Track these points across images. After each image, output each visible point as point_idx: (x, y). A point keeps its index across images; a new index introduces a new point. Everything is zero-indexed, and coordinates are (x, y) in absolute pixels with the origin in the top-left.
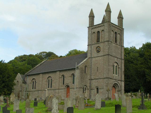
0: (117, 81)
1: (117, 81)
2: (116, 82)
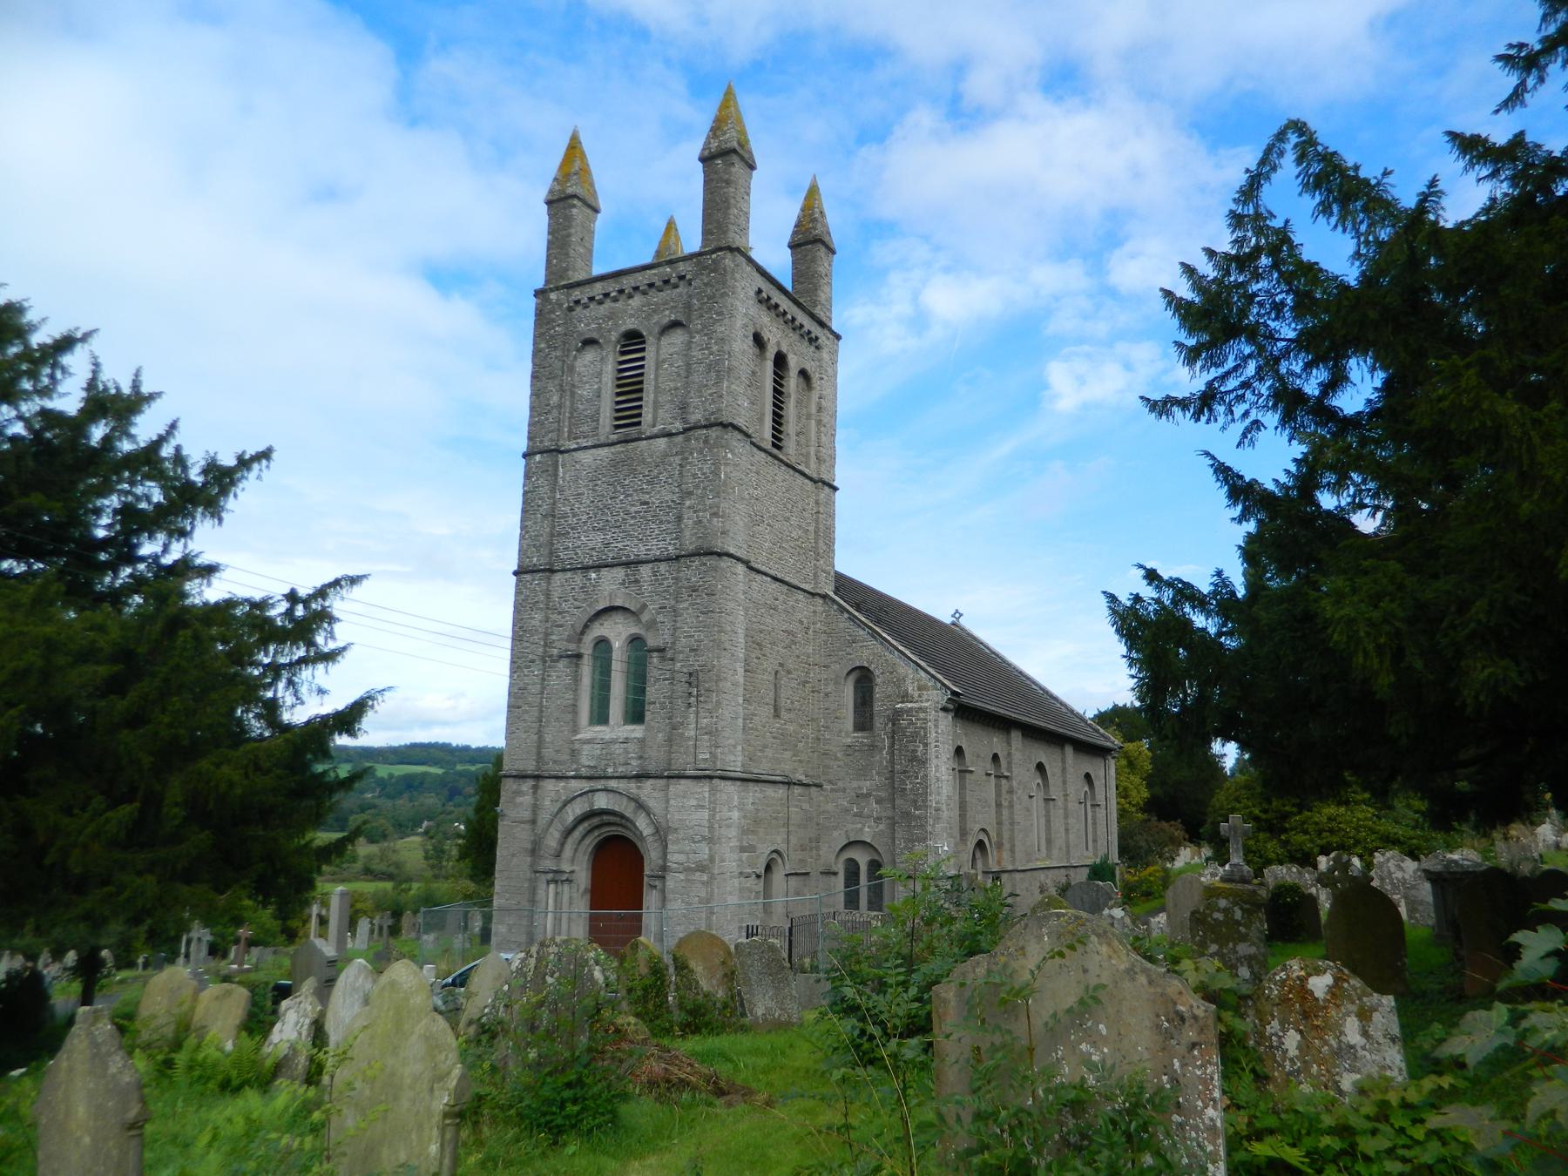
0: (613, 784)
1: (632, 787)
2: (601, 802)
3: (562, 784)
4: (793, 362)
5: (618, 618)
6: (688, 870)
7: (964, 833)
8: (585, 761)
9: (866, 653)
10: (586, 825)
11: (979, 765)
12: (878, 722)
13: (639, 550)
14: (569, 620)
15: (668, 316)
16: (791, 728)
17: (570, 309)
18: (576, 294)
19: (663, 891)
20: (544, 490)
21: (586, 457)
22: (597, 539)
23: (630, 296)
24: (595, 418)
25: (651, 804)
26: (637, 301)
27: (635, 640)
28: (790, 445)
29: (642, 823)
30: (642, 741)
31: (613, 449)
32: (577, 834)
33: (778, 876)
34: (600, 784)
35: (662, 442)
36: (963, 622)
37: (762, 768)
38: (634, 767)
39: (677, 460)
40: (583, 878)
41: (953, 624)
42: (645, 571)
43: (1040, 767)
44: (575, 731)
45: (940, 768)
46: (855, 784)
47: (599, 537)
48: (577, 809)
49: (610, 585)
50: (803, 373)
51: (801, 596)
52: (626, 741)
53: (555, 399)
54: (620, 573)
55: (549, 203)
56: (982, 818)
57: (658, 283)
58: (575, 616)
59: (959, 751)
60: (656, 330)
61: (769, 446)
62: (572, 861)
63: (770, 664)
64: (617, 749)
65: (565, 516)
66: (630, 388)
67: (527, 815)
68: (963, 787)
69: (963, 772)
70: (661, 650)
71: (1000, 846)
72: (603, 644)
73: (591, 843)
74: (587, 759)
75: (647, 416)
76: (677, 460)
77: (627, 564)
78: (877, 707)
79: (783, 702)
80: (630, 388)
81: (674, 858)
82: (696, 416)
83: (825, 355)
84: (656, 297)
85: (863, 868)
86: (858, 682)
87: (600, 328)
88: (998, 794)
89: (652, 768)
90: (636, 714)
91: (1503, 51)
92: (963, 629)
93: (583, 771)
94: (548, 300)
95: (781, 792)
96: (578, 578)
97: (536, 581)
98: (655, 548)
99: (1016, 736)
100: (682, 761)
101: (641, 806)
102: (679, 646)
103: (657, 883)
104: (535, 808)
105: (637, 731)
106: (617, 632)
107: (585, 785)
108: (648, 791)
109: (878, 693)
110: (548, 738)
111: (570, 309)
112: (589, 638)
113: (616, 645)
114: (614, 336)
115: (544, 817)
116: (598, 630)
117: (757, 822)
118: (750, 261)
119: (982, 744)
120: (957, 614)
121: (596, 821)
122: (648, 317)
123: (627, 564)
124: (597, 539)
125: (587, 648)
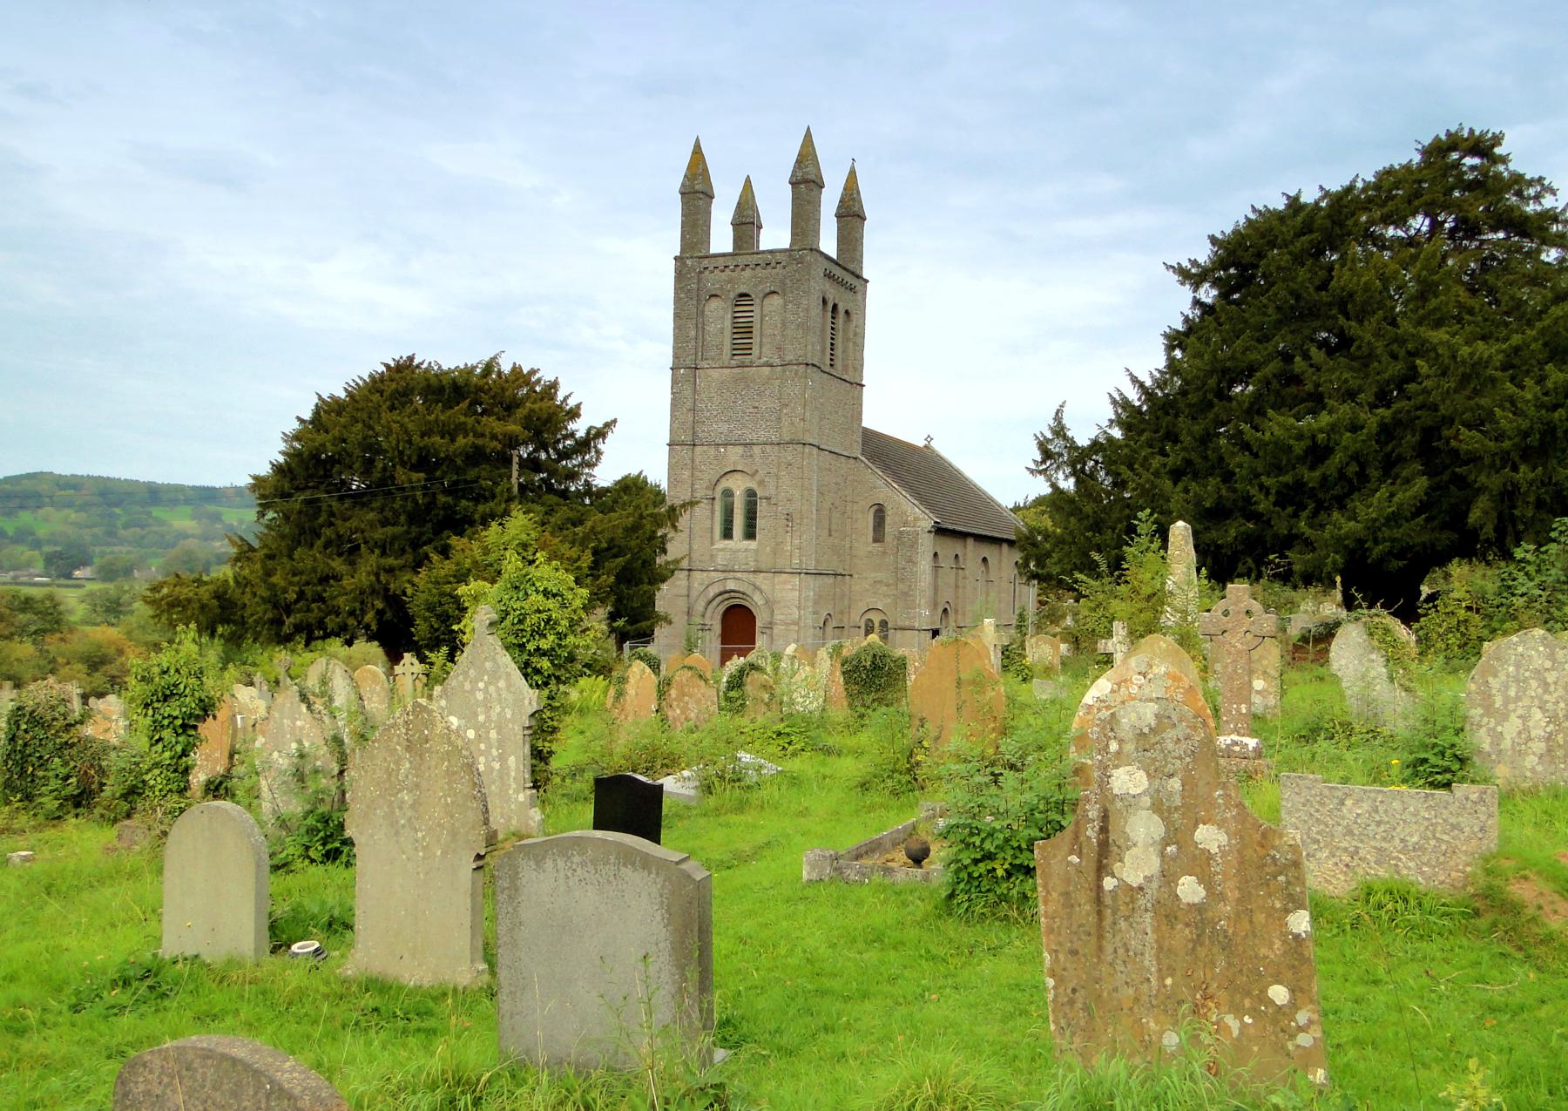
2: (731, 585)
3: (705, 574)
4: (841, 309)
5: (737, 476)
6: (786, 624)
7: (935, 604)
8: (719, 561)
9: (882, 495)
10: (720, 598)
11: (946, 562)
12: (888, 538)
13: (754, 437)
14: (706, 476)
15: (769, 287)
16: (836, 541)
17: (701, 272)
18: (705, 263)
19: (771, 635)
20: (688, 392)
21: (715, 374)
22: (724, 428)
23: (743, 270)
24: (720, 348)
25: (764, 587)
26: (748, 273)
27: (751, 494)
28: (838, 363)
29: (757, 598)
30: (757, 551)
31: (734, 370)
32: (715, 603)
33: (829, 629)
34: (731, 575)
35: (766, 370)
36: (934, 445)
37: (823, 568)
38: (752, 565)
39: (777, 382)
40: (717, 628)
41: (926, 446)
42: (757, 449)
43: (985, 560)
44: (712, 544)
45: (924, 564)
46: (873, 575)
47: (726, 426)
48: (712, 592)
49: (734, 455)
50: (847, 312)
51: (843, 459)
52: (746, 550)
53: (693, 333)
54: (740, 450)
55: (682, 194)
56: (947, 595)
57: (763, 265)
58: (710, 474)
59: (936, 554)
60: (762, 295)
61: (828, 369)
62: (712, 618)
63: (827, 505)
64: (741, 555)
65: (702, 411)
66: (743, 331)
67: (685, 592)
68: (936, 577)
69: (937, 568)
70: (768, 499)
71: (956, 612)
72: (728, 493)
73: (722, 609)
74: (720, 560)
75: (755, 351)
76: (777, 382)
77: (745, 445)
78: (888, 529)
79: (834, 527)
80: (743, 331)
81: (778, 617)
82: (789, 357)
83: (859, 297)
84: (760, 272)
85: (877, 624)
86: (876, 511)
87: (721, 288)
88: (957, 580)
89: (763, 567)
90: (750, 534)
91: (1186, 264)
92: (933, 451)
93: (719, 567)
94: (684, 264)
95: (831, 580)
96: (712, 451)
97: (685, 452)
98: (762, 435)
99: (970, 541)
100: (781, 563)
101: (756, 587)
102: (780, 498)
103: (767, 631)
104: (689, 588)
105: (752, 545)
106: (738, 486)
107: (721, 576)
108: (760, 579)
109: (888, 520)
110: (695, 547)
111: (701, 272)
112: (720, 489)
113: (738, 493)
114: (732, 295)
115: (694, 594)
116: (724, 484)
117: (820, 596)
118: (822, 253)
119: (949, 548)
120: (929, 438)
121: (727, 596)
122: (755, 286)
123: (745, 445)
124: (724, 428)
125: (718, 495)
